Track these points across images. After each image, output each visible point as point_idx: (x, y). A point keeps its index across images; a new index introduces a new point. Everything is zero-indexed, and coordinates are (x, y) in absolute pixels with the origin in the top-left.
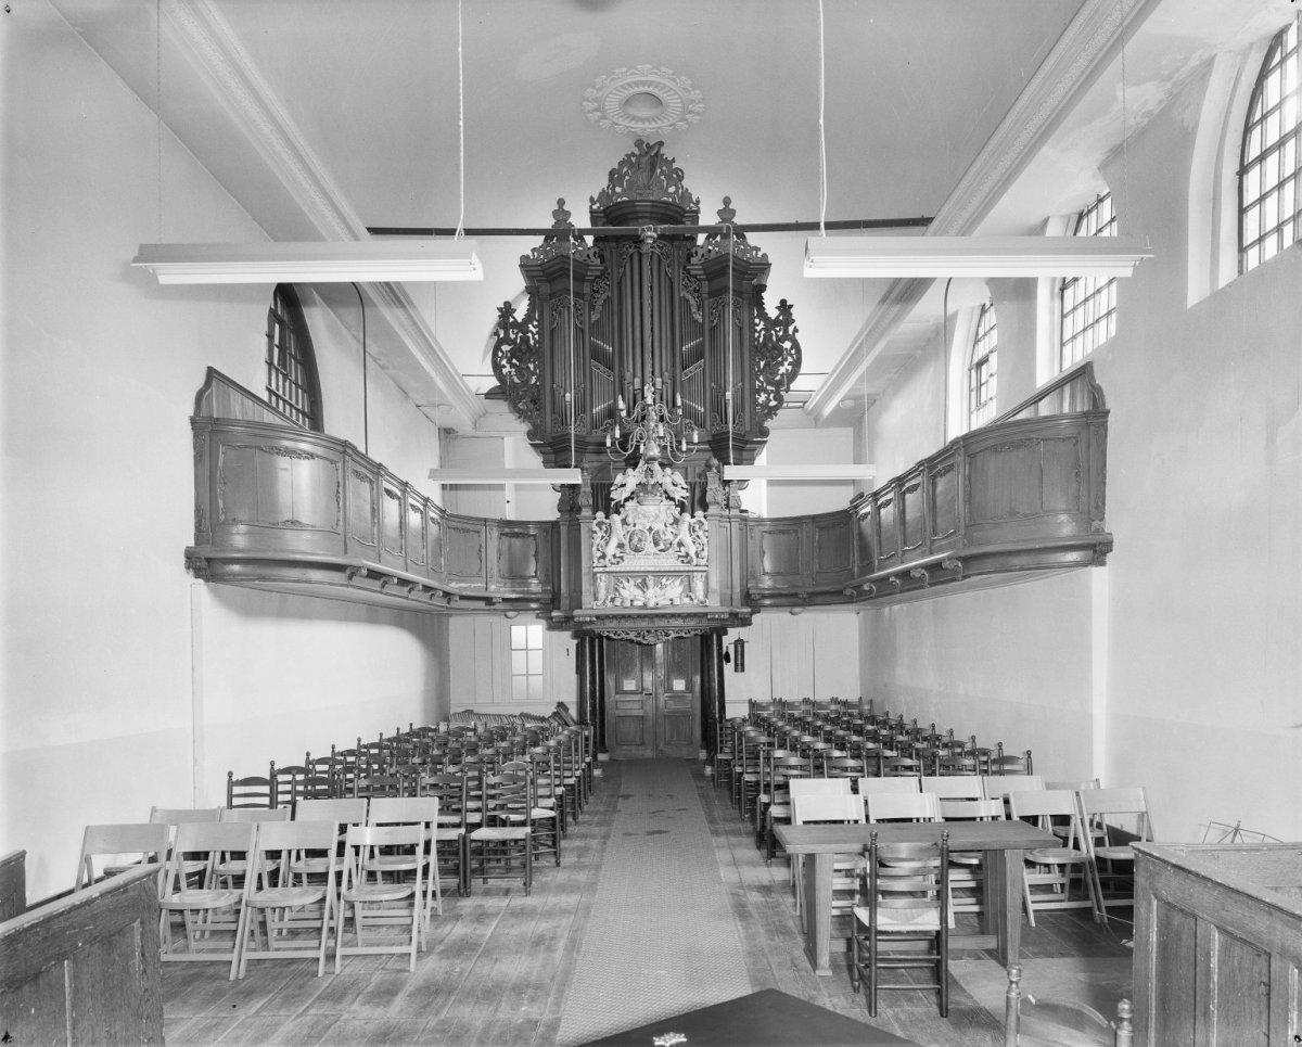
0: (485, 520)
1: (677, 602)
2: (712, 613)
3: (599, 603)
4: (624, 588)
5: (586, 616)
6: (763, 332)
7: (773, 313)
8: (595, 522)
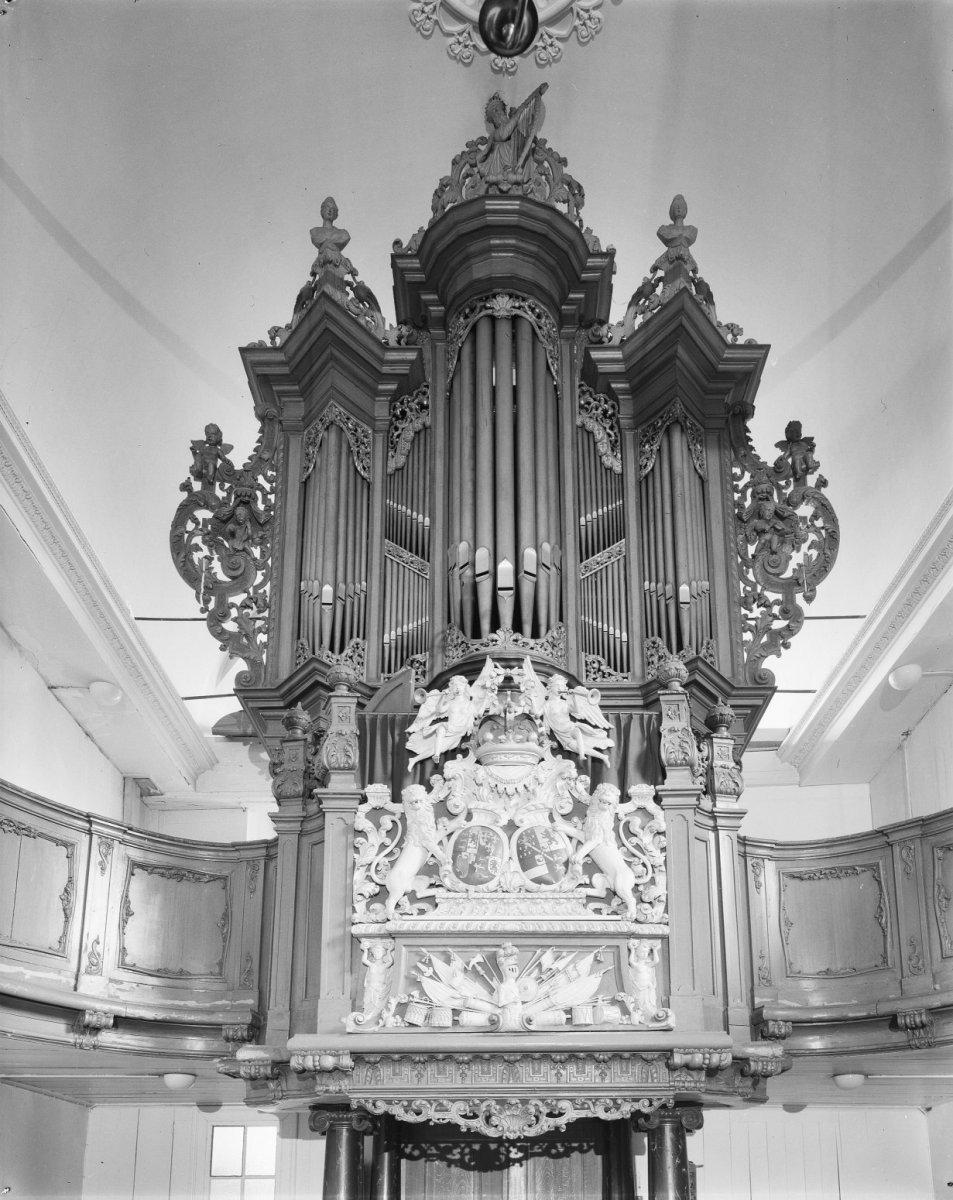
0: (88, 818)
1: (584, 1016)
2: (687, 1050)
3: (367, 1017)
4: (435, 976)
5: (325, 1051)
6: (749, 491)
7: (767, 449)
8: (365, 808)
